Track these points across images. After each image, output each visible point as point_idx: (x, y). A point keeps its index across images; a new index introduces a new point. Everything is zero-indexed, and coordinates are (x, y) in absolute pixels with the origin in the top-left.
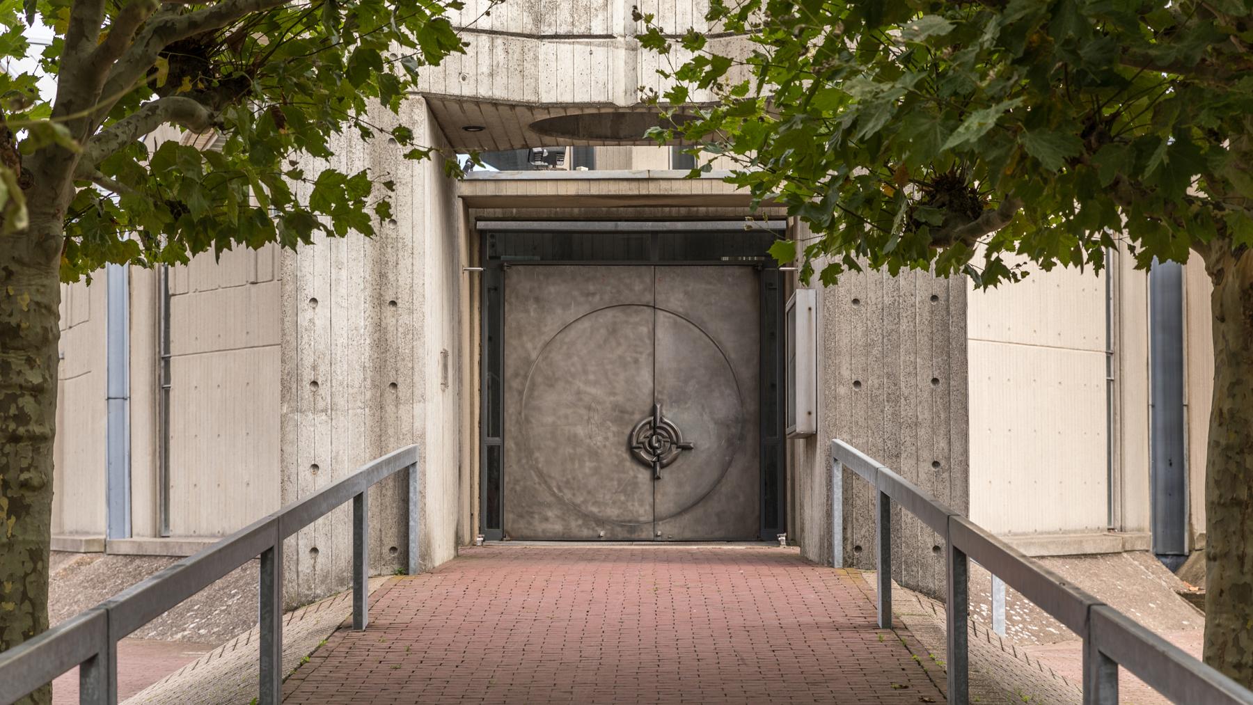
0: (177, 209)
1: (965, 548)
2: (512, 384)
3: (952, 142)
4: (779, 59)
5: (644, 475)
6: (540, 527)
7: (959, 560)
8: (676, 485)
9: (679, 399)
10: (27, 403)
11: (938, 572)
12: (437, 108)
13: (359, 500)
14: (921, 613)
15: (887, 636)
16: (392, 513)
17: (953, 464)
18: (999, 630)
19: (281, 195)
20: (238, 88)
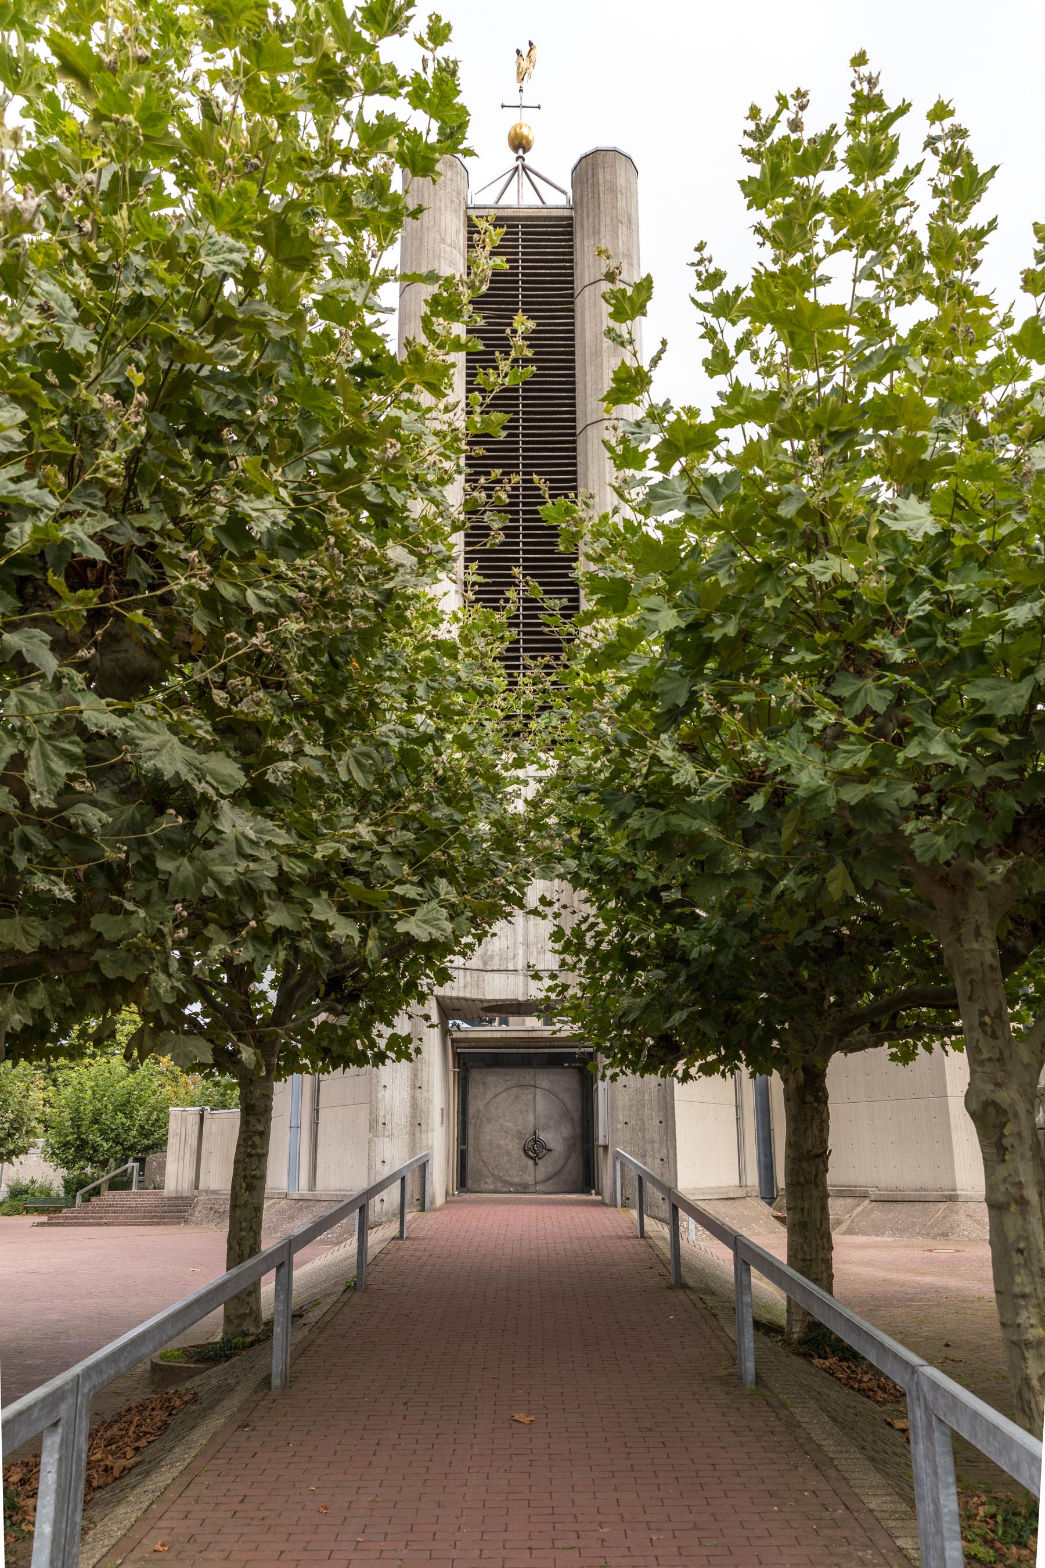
0: (326, 1051)
1: (677, 1204)
2: (472, 1121)
3: (668, 1025)
4: (590, 985)
5: (531, 1163)
6: (484, 1187)
7: (675, 1209)
8: (546, 1167)
9: (546, 1128)
10: (257, 1139)
11: (665, 1210)
12: (441, 1002)
13: (403, 1179)
14: (657, 1229)
15: (643, 1242)
16: (418, 1182)
17: (669, 1161)
18: (692, 1236)
19: (373, 1044)
20: (354, 998)
